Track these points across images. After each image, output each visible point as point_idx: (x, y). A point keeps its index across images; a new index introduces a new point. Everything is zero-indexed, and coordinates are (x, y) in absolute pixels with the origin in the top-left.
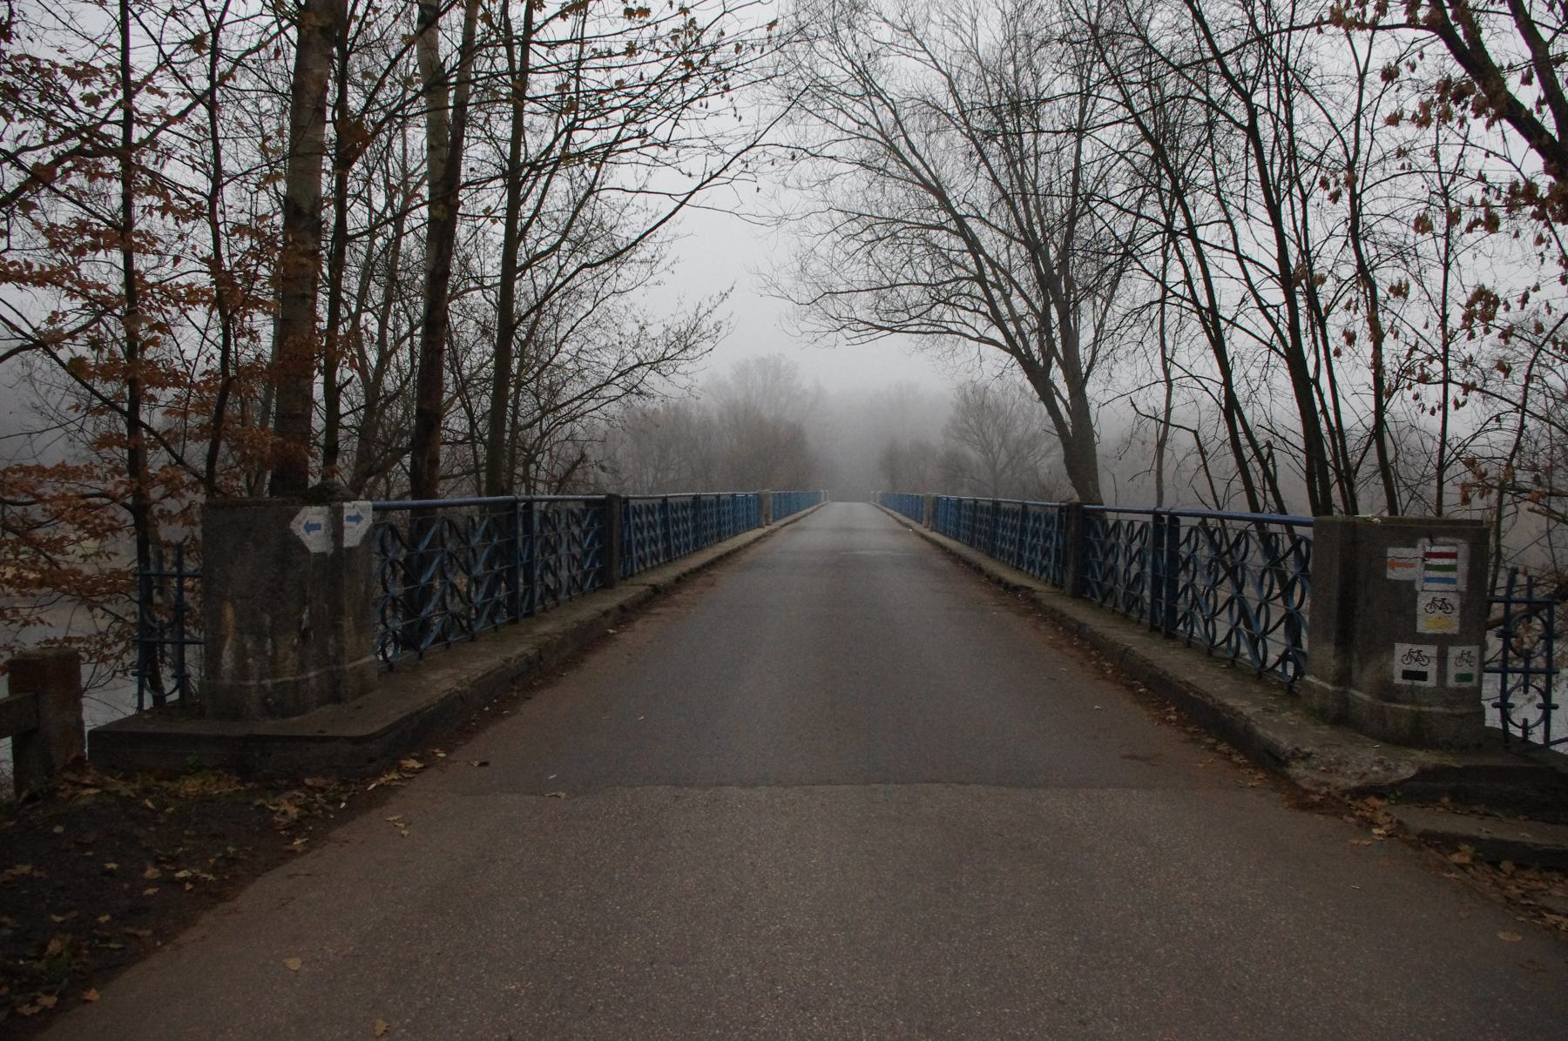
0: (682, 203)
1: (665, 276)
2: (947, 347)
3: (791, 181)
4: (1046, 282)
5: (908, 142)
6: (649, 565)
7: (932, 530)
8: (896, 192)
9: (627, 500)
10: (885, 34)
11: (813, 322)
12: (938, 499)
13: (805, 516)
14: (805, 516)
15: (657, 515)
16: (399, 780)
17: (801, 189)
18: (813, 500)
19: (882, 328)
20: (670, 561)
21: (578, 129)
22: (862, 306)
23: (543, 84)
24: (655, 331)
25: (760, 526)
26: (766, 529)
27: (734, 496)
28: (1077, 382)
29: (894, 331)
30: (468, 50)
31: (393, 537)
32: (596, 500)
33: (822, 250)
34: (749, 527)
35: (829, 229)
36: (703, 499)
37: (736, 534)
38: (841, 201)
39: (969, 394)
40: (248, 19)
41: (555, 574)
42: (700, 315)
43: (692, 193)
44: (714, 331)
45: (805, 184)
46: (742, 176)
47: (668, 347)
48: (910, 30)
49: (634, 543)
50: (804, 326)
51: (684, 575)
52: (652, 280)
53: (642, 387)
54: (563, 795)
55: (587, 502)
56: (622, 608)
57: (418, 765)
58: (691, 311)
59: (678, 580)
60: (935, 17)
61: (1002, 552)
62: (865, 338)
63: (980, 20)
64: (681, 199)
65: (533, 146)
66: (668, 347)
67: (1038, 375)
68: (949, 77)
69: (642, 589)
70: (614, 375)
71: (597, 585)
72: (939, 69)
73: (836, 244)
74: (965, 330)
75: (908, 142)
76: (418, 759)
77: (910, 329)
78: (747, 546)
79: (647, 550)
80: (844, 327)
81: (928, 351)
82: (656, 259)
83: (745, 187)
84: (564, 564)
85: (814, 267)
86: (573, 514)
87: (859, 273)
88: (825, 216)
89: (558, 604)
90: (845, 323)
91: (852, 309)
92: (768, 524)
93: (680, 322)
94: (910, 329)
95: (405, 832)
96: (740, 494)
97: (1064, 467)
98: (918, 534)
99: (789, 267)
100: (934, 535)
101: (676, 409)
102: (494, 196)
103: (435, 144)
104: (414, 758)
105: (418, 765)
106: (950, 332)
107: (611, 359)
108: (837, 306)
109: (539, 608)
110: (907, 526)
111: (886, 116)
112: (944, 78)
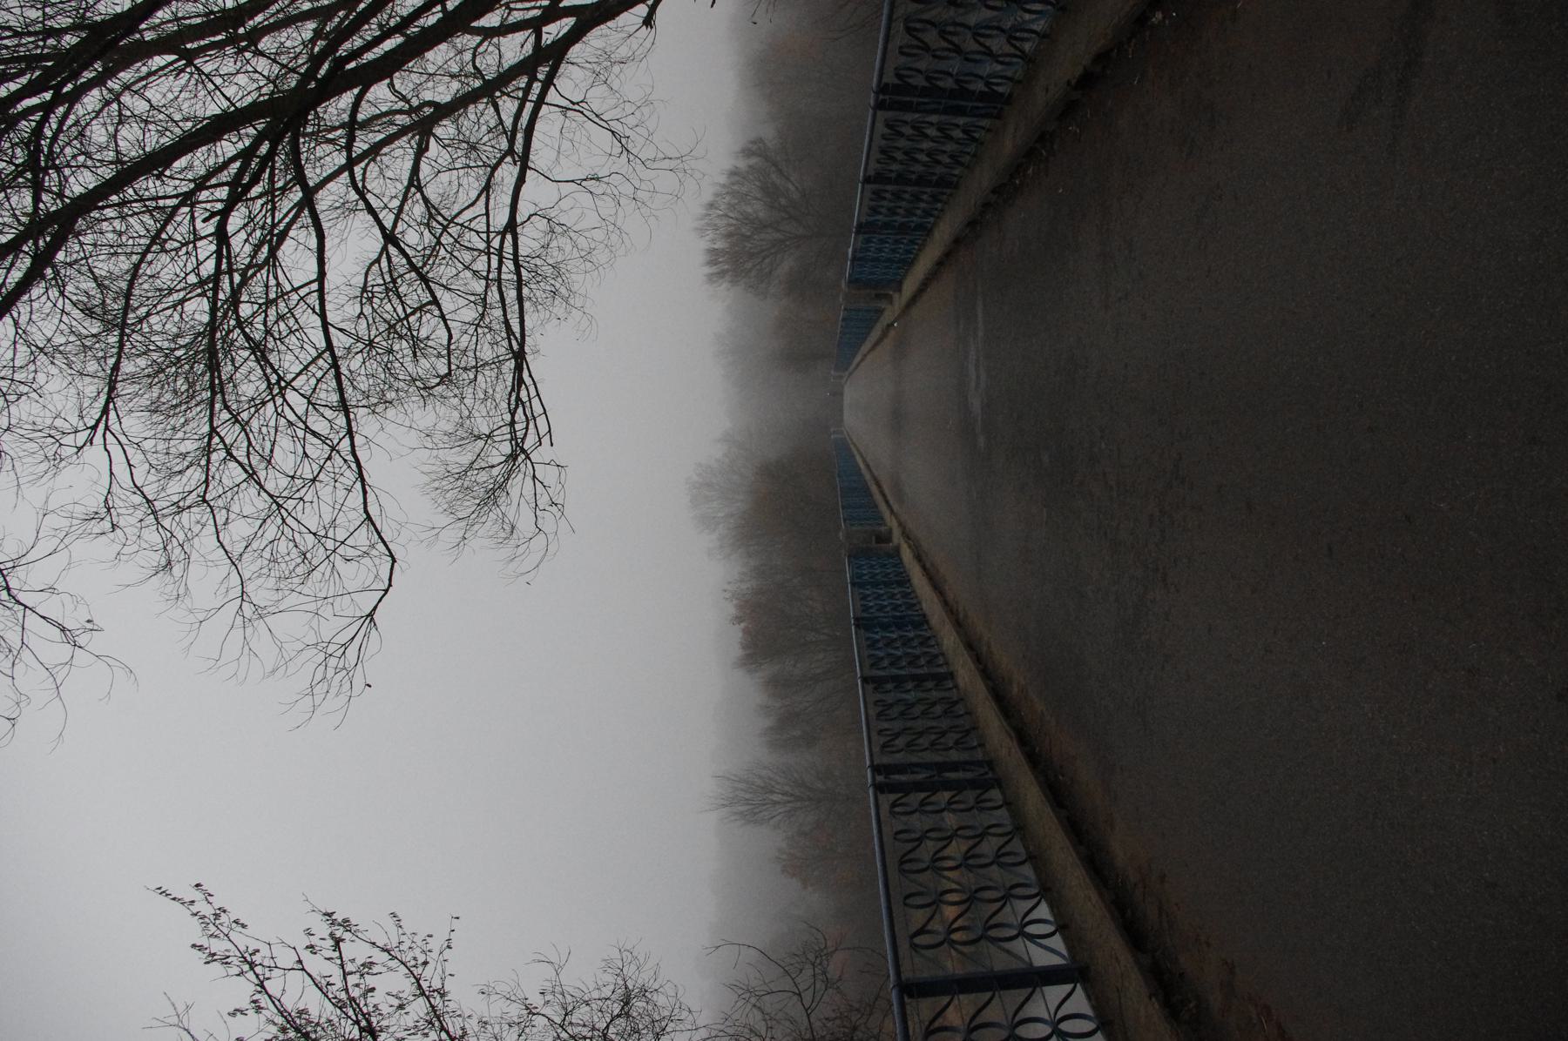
12: (854, 282)
14: (864, 461)
18: (844, 449)
31: (888, 746)
40: (297, 520)
62: (538, 409)
84: (909, 724)
100: (909, 287)
101: (740, 607)
102: (384, 271)
110: (884, 334)
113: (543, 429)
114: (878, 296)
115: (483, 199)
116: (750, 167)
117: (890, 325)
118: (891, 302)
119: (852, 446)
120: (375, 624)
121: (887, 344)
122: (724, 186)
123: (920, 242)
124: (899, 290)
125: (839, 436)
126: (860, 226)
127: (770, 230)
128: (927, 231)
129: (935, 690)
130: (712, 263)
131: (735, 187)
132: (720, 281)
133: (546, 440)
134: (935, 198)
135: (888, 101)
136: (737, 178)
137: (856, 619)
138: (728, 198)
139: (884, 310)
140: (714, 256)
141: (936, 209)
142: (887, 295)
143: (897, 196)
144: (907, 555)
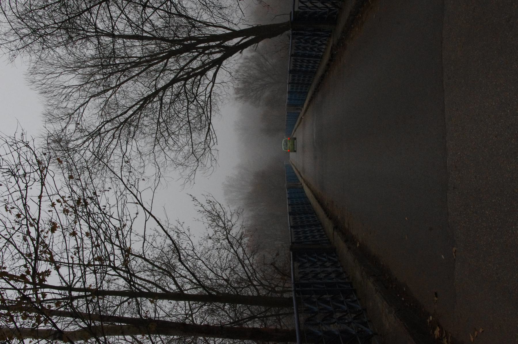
0: (150, 213)
1: (185, 226)
2: (217, 98)
3: (141, 170)
4: (188, 49)
5: (121, 115)
6: (323, 233)
7: (303, 107)
8: (146, 121)
9: (293, 243)
10: (72, 127)
11: (207, 161)
13: (297, 170)
14: (297, 170)
15: (299, 230)
16: (447, 339)
17: (144, 166)
18: (289, 167)
19: (209, 129)
20: (321, 224)
21: (114, 264)
22: (199, 137)
23: (91, 280)
24: (211, 232)
25: (302, 188)
26: (304, 185)
27: (288, 198)
28: (235, 34)
29: (210, 122)
30: (75, 315)
32: (293, 256)
33: (172, 155)
34: (303, 192)
35: (163, 153)
36: (290, 211)
37: (307, 197)
38: (149, 147)
39: (238, 96)
41: (330, 273)
42: (203, 210)
43: (144, 208)
44: (211, 203)
45: (142, 164)
46: (137, 187)
47: (219, 226)
48: (70, 115)
49: (313, 239)
50: (209, 165)
51: (328, 216)
52: (187, 232)
53: (238, 237)
54: (454, 249)
55: (294, 260)
56: (346, 241)
57: (438, 329)
58: (201, 215)
59: (330, 218)
60: (64, 105)
61: (313, 67)
62: (214, 136)
63: (65, 85)
64: (148, 214)
65: (121, 284)
66: (219, 226)
67: (229, 52)
68: (91, 97)
69: (336, 233)
70: (232, 250)
71: (334, 255)
72: (87, 102)
73: (169, 149)
74: (209, 89)
75: (121, 115)
76: (434, 329)
77: (209, 115)
78: (312, 191)
79: (316, 234)
80: (209, 146)
81: (220, 107)
82: (177, 230)
83: (142, 185)
85: (180, 158)
86: (300, 266)
87: (183, 140)
88: (157, 154)
89: (345, 272)
90: (207, 147)
91: (200, 143)
92: (301, 184)
93: (207, 221)
94: (209, 115)
95: (481, 331)
96: (287, 196)
97: (272, 38)
98: (304, 115)
99: (181, 171)
103: (121, 331)
104: (433, 332)
105: (438, 329)
106: (210, 96)
107: (224, 253)
108: (199, 151)
109: (347, 280)
110: (301, 121)
111: (108, 126)
112: (92, 99)
113: (215, 141)
114: (297, 109)
115: (205, 91)
116: (252, 56)
117: (302, 118)
119: (292, 165)
120: (195, 173)
121: (301, 125)
122: (242, 63)
125: (288, 163)
127: (260, 81)
128: (307, 93)
130: (236, 93)
131: (247, 64)
132: (241, 100)
133: (216, 144)
136: (247, 60)
137: (289, 212)
138: (244, 68)
139: (300, 113)
140: (238, 91)
142: (300, 109)
143: (309, 61)
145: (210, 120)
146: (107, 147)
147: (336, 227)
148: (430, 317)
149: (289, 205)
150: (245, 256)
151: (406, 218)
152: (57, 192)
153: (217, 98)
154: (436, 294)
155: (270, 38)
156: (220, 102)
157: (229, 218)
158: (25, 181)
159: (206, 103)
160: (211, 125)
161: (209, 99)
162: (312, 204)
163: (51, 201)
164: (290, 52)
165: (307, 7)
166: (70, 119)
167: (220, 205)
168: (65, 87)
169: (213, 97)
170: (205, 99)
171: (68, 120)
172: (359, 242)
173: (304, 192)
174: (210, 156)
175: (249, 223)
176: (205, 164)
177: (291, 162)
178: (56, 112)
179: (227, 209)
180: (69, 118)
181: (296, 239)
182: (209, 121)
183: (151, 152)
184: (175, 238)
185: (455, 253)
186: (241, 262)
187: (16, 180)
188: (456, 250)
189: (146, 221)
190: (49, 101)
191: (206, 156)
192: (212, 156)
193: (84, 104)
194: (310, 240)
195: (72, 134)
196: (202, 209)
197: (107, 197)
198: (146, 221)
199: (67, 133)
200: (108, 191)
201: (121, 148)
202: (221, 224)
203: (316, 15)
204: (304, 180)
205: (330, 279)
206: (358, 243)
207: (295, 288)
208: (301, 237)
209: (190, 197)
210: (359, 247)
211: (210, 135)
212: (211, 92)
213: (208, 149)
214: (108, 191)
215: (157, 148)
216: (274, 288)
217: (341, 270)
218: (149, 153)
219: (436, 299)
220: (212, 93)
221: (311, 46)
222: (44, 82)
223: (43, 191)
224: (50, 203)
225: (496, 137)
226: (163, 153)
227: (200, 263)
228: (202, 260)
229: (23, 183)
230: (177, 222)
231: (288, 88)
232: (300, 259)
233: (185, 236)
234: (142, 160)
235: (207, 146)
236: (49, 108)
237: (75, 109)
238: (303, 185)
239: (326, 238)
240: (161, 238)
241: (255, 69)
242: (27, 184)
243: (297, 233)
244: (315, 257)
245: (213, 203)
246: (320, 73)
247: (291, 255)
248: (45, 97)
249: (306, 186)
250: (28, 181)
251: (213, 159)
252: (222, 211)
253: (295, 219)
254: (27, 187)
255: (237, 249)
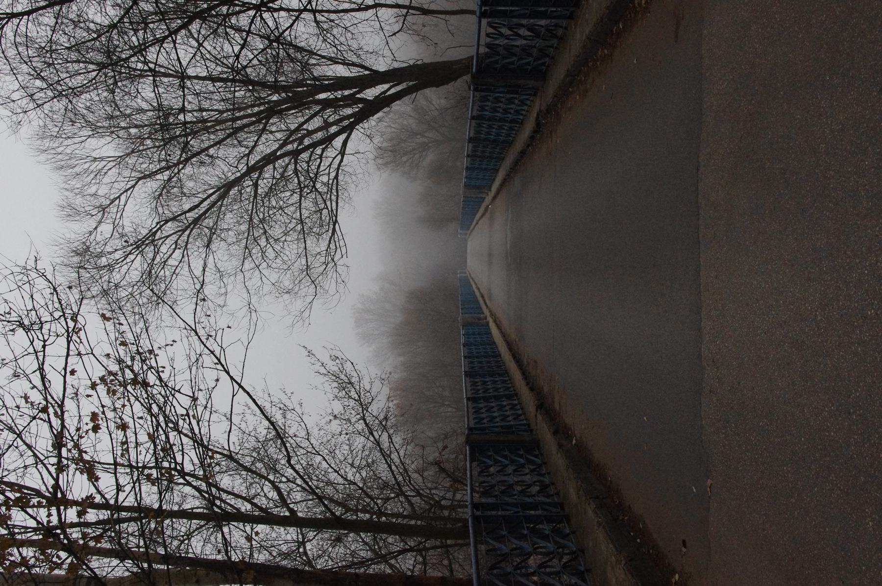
0: (240, 386)
3: (220, 301)
5: (190, 210)
6: (520, 412)
8: (229, 219)
9: (470, 429)
10: (106, 229)
11: (329, 284)
12: (466, 185)
13: (478, 289)
15: (481, 405)
17: (226, 293)
18: (466, 283)
19: (334, 230)
20: (516, 395)
22: (317, 246)
25: (488, 323)
29: (336, 220)
33: (274, 277)
34: (489, 333)
37: (494, 343)
38: (236, 263)
42: (325, 372)
43: (232, 378)
44: (337, 361)
45: (223, 291)
48: (103, 209)
50: (332, 290)
51: (528, 384)
52: (298, 409)
53: (381, 417)
54: (709, 482)
55: (472, 461)
56: (555, 433)
60: (93, 190)
61: (508, 135)
62: (342, 243)
63: (95, 155)
64: (236, 387)
66: (350, 397)
67: (371, 108)
68: (140, 179)
69: (540, 417)
70: (372, 439)
71: (537, 453)
72: (133, 186)
73: (269, 266)
74: (335, 166)
75: (190, 210)
78: (503, 334)
79: (508, 413)
80: (333, 259)
81: (352, 194)
82: (282, 406)
85: (287, 283)
87: (292, 249)
88: (247, 275)
89: (553, 484)
92: (486, 318)
93: (330, 387)
100: (494, 188)
103: (194, 579)
106: (336, 177)
107: (359, 441)
112: (140, 182)
118: (488, 195)
119: (471, 280)
121: (487, 215)
123: (528, 102)
124: (490, 190)
126: (467, 168)
128: (497, 171)
129: (538, 496)
133: (345, 256)
134: (511, 129)
135: (489, 11)
137: (465, 372)
139: (485, 198)
141: (524, 110)
143: (501, 128)
144: (492, 326)
145: (336, 217)
146: (165, 262)
147: (540, 407)
148: (675, 575)
149: (465, 357)
150: (392, 446)
151: (645, 418)
152: (90, 350)
153: (348, 179)
154: (684, 542)
155: (437, 86)
156: (353, 186)
157: (368, 387)
158: (41, 337)
159: (330, 186)
160: (337, 224)
161: (335, 181)
162: (502, 356)
163: (90, 379)
164: (470, 113)
165: (501, 35)
166: (104, 214)
167: (352, 364)
168: (95, 159)
169: (340, 178)
170: (328, 181)
171: (100, 217)
172: (575, 436)
173: (491, 333)
174: (334, 276)
175: (396, 376)
176: (327, 288)
177: (470, 274)
178: (78, 201)
179: (364, 372)
180: (102, 212)
181: (473, 392)
182: (334, 218)
183: (238, 270)
184: (278, 417)
185: (710, 488)
186: (385, 456)
187: (30, 339)
188: (711, 484)
189: (233, 396)
190: (69, 182)
191: (329, 277)
192: (338, 276)
193: (126, 191)
194: (499, 424)
195: (107, 240)
196: (323, 370)
197: (169, 357)
198: (233, 396)
199: (99, 238)
200: (172, 345)
201: (189, 266)
202: (353, 394)
203: (513, 66)
204: (490, 311)
205: (529, 496)
206: (574, 438)
207: (473, 512)
208: (483, 419)
209: (304, 349)
210: (575, 444)
211: (335, 242)
212: (338, 169)
213: (331, 265)
214: (172, 345)
215: (248, 265)
216: (439, 502)
217: (547, 480)
218: (234, 272)
219: (684, 550)
220: (340, 171)
221: (505, 106)
222: (59, 150)
223: (71, 349)
224: (89, 383)
225: (765, 333)
226: (257, 272)
227: (318, 459)
228: (322, 456)
229: (39, 340)
230: (282, 392)
231: (467, 148)
232: (482, 459)
233: (294, 416)
234: (222, 283)
235: (330, 259)
236: (67, 193)
237: (112, 197)
238: (488, 319)
239: (525, 422)
240: (256, 418)
241: (411, 116)
242: (45, 341)
243: (477, 411)
244: (505, 457)
245: (341, 360)
246: (519, 145)
247: (468, 455)
248: (60, 175)
249: (494, 324)
250: (46, 337)
251: (339, 280)
252: (356, 375)
253: (474, 384)
254: (44, 346)
255: (380, 436)
